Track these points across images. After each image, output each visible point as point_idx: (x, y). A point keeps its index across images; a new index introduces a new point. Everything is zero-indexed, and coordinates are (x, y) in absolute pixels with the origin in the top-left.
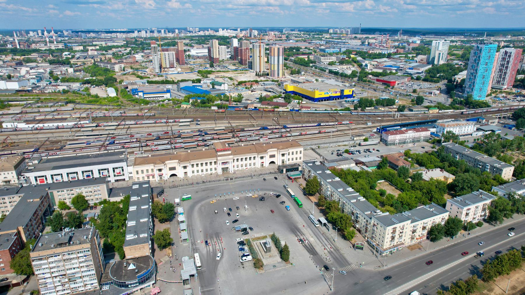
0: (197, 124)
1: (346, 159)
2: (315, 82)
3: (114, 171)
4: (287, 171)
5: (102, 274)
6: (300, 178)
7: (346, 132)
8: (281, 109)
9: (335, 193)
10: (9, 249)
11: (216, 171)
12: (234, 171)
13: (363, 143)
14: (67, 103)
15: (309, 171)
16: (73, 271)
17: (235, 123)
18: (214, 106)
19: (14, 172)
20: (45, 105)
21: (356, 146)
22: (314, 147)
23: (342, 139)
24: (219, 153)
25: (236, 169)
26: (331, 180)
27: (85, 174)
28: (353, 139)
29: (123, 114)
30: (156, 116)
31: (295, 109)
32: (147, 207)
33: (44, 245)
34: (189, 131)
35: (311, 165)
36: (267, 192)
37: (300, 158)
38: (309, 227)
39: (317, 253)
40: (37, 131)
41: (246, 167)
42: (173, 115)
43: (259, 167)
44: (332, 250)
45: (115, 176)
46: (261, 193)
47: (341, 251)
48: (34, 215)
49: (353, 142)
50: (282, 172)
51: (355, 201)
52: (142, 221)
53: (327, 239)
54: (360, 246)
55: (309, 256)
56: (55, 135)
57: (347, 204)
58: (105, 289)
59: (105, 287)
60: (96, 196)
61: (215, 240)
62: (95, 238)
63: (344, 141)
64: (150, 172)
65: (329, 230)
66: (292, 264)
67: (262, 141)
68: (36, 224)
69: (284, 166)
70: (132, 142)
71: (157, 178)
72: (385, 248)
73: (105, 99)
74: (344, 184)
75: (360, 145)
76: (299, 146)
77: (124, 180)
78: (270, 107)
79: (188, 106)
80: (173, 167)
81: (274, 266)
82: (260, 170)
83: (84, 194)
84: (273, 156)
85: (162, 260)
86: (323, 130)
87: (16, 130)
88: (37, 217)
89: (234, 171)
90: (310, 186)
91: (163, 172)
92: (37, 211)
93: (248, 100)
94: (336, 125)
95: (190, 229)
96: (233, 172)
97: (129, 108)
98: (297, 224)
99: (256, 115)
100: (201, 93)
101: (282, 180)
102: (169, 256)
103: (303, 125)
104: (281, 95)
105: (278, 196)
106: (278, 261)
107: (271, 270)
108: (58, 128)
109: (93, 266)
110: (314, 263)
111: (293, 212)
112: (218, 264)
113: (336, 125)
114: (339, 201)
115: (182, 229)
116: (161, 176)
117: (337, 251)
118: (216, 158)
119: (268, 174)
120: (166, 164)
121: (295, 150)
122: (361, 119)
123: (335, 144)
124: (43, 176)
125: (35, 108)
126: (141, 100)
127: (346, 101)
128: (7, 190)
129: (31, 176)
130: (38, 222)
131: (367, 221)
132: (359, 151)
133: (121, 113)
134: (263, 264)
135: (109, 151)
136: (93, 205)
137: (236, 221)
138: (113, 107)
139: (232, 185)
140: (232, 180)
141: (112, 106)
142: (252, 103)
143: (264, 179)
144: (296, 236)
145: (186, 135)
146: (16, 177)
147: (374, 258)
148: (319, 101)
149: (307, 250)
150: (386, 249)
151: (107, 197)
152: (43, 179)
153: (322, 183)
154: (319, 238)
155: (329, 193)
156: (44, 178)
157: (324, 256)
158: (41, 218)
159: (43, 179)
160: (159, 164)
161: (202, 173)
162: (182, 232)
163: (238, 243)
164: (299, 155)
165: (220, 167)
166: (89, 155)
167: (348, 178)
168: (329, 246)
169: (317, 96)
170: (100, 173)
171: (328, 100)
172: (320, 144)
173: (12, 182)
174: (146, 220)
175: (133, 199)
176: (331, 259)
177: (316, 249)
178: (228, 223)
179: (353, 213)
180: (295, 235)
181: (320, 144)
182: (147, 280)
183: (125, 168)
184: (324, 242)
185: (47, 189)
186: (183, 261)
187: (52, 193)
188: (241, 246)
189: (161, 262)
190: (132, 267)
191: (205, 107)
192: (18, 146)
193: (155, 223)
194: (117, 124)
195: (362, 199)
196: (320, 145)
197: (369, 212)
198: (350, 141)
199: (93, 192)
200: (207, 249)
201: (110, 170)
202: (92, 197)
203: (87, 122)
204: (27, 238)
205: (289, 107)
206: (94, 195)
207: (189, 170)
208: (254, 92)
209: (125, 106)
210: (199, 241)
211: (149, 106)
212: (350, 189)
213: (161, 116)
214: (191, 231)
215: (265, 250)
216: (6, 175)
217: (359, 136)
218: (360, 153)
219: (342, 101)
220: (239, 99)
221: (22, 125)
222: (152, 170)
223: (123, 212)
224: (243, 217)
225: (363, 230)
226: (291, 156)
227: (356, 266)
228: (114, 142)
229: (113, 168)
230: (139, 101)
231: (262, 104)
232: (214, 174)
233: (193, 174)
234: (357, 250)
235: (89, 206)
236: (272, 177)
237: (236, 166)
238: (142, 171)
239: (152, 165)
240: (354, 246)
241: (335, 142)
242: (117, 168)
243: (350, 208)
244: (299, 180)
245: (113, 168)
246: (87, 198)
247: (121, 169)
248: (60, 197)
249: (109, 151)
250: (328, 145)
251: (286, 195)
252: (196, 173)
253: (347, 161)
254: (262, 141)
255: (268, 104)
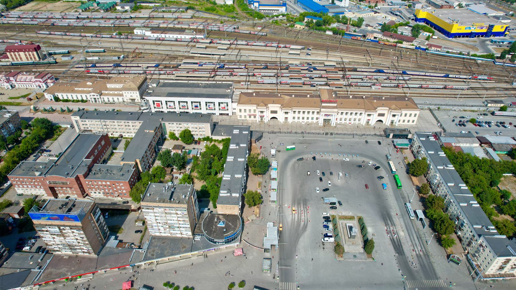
0: (308, 54)
1: (469, 135)
2: (457, 8)
3: (219, 105)
4: (395, 136)
5: (196, 224)
6: (407, 148)
7: (480, 92)
8: (405, 45)
9: (443, 185)
10: (129, 182)
11: (317, 121)
12: (337, 124)
13: (497, 113)
14: (187, 9)
15: (419, 147)
16: (172, 222)
17: (348, 58)
18: (329, 30)
19: (138, 92)
20: (169, 10)
21: (487, 115)
22: (432, 107)
23: (470, 102)
24: (323, 105)
25: (339, 122)
26: (442, 168)
27: (194, 104)
28: (486, 105)
29: (236, 30)
30: (268, 36)
31: (422, 47)
32: (243, 160)
33: (151, 195)
34: (297, 62)
35: (424, 139)
36: (366, 160)
37: (413, 121)
38: (403, 217)
39: (403, 252)
40: (159, 42)
41: (350, 122)
42: (285, 37)
43: (364, 125)
44: (421, 253)
45: (220, 109)
46: (359, 159)
47: (431, 257)
48: (148, 147)
49: (485, 108)
50: (387, 136)
51: (466, 205)
52: (236, 176)
53: (419, 238)
54: (455, 259)
55: (394, 254)
56: (174, 48)
57: (454, 204)
58: (197, 239)
59: (197, 238)
60: (201, 132)
61: (302, 209)
62: (192, 196)
63: (472, 106)
64: (252, 113)
65: (424, 227)
66: (373, 259)
67: (374, 88)
68: (150, 154)
69: (393, 130)
70: (240, 68)
71: (258, 119)
72: (487, 273)
73: (222, 6)
74: (457, 175)
75: (493, 114)
76: (415, 106)
77: (228, 114)
78: (392, 40)
79: (302, 27)
80: (274, 111)
81: (355, 256)
82: (365, 128)
83: (190, 129)
84: (382, 115)
85: (249, 218)
86: (450, 84)
87: (143, 39)
88: (151, 148)
89: (337, 124)
90: (416, 167)
91: (264, 114)
92: (151, 142)
93: (369, 26)
94: (469, 79)
95: (280, 189)
96: (334, 125)
97: (243, 22)
98: (391, 210)
99: (373, 49)
100: (317, 11)
101: (386, 148)
102: (256, 216)
103: (427, 74)
104: (409, 23)
105: (377, 168)
106: (360, 252)
107: (350, 260)
108: (177, 40)
109: (189, 222)
110: (397, 265)
111: (389, 192)
112: (300, 237)
113: (469, 79)
114: (446, 196)
115: (272, 188)
116: (262, 117)
117: (427, 257)
118: (319, 109)
119: (372, 135)
120: (268, 107)
121: (408, 112)
122: (506, 74)
123: (460, 108)
124: (159, 101)
125: (161, 12)
126: (256, 13)
127: (492, 41)
128: (131, 114)
129: (150, 99)
130: (152, 152)
131: (474, 236)
132: (489, 123)
133: (234, 28)
134: (344, 251)
135: (218, 82)
136: (197, 139)
137: (327, 190)
138: (228, 19)
139: (331, 142)
140: (331, 136)
141: (227, 17)
142: (373, 32)
143: (367, 142)
144: (386, 225)
145: (294, 69)
146: (139, 97)
147: (470, 280)
148: (456, 37)
149: (393, 245)
150: (489, 275)
151: (209, 134)
152: (159, 104)
153: (431, 167)
154: (411, 235)
155: (436, 181)
156: (160, 103)
157: (410, 259)
158: (155, 148)
159: (159, 104)
160: (262, 106)
161: (303, 120)
162: (272, 190)
163: (324, 217)
164: (412, 118)
165: (322, 118)
166: (199, 84)
167: (465, 167)
168: (419, 248)
169: (454, 31)
170: (206, 105)
171: (467, 37)
172: (441, 105)
173: (136, 101)
174: (240, 176)
175: (232, 146)
176: (418, 265)
177: (404, 247)
178: (318, 190)
179: (458, 218)
180: (385, 223)
181: (441, 105)
182: (233, 240)
183: (230, 104)
184: (414, 240)
185: (161, 120)
186: (268, 226)
187: (164, 124)
188: (326, 223)
189: (248, 220)
190: (221, 225)
191: (319, 30)
192: (144, 57)
193: (249, 174)
194: (229, 43)
195: (475, 204)
196: (440, 107)
197: (480, 227)
198: (481, 106)
199: (198, 128)
200: (292, 217)
201: (215, 104)
202: (197, 133)
203: (202, 37)
204: (142, 168)
205: (415, 43)
206: (198, 131)
207: (290, 116)
208: (377, 14)
209: (239, 19)
210: (286, 205)
211: (262, 20)
212: (464, 186)
213: (273, 36)
214: (281, 190)
215: (349, 236)
216: (132, 94)
217: (496, 102)
218: (489, 126)
219: (487, 40)
220: (359, 23)
221: (148, 33)
222: (255, 111)
223: (222, 155)
224: (334, 186)
225: (466, 241)
226: (403, 118)
227: (444, 282)
228: (224, 67)
229: (219, 103)
230: (254, 14)
231: (384, 35)
232: (315, 124)
233: (294, 120)
234: (451, 262)
235: (194, 140)
236: (376, 140)
237: (339, 119)
238: (245, 110)
239: (255, 105)
240: (448, 256)
241: (461, 106)
242: (222, 103)
243: (456, 211)
244: (405, 151)
245: (219, 103)
246: (192, 133)
247: (226, 104)
248: (170, 128)
249: (218, 82)
250: (451, 107)
251: (386, 167)
252: (296, 120)
253: (469, 139)
254: (374, 88)
255: (391, 36)
